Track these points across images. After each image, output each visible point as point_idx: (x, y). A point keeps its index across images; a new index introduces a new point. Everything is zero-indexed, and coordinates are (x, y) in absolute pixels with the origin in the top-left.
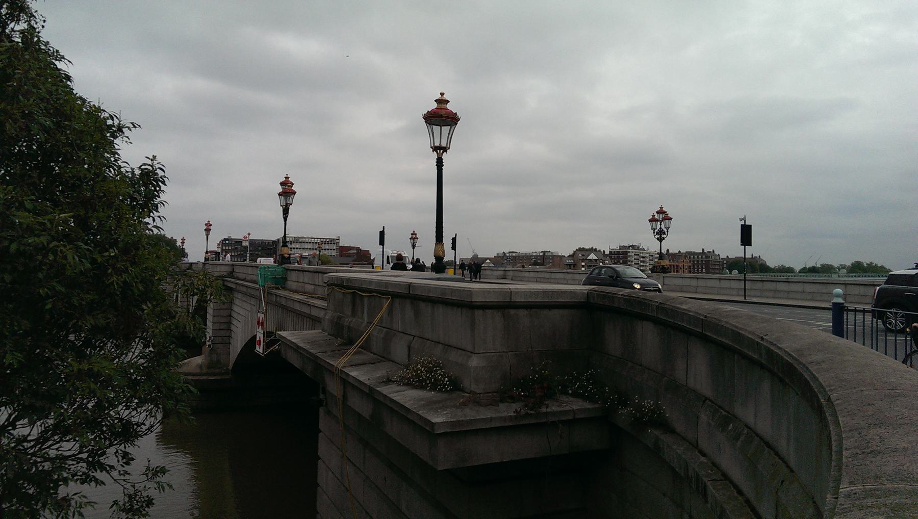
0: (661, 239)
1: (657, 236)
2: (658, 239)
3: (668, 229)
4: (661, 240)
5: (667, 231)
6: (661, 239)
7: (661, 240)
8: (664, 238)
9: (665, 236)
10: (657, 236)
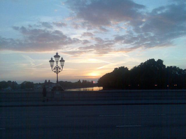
0: (57, 72)
1: (54, 70)
2: (55, 72)
3: (62, 66)
4: (57, 73)
5: (62, 68)
6: (57, 72)
7: (57, 73)
8: (60, 72)
9: (60, 70)
10: (54, 70)
